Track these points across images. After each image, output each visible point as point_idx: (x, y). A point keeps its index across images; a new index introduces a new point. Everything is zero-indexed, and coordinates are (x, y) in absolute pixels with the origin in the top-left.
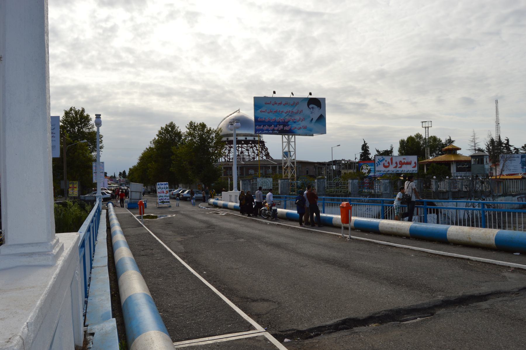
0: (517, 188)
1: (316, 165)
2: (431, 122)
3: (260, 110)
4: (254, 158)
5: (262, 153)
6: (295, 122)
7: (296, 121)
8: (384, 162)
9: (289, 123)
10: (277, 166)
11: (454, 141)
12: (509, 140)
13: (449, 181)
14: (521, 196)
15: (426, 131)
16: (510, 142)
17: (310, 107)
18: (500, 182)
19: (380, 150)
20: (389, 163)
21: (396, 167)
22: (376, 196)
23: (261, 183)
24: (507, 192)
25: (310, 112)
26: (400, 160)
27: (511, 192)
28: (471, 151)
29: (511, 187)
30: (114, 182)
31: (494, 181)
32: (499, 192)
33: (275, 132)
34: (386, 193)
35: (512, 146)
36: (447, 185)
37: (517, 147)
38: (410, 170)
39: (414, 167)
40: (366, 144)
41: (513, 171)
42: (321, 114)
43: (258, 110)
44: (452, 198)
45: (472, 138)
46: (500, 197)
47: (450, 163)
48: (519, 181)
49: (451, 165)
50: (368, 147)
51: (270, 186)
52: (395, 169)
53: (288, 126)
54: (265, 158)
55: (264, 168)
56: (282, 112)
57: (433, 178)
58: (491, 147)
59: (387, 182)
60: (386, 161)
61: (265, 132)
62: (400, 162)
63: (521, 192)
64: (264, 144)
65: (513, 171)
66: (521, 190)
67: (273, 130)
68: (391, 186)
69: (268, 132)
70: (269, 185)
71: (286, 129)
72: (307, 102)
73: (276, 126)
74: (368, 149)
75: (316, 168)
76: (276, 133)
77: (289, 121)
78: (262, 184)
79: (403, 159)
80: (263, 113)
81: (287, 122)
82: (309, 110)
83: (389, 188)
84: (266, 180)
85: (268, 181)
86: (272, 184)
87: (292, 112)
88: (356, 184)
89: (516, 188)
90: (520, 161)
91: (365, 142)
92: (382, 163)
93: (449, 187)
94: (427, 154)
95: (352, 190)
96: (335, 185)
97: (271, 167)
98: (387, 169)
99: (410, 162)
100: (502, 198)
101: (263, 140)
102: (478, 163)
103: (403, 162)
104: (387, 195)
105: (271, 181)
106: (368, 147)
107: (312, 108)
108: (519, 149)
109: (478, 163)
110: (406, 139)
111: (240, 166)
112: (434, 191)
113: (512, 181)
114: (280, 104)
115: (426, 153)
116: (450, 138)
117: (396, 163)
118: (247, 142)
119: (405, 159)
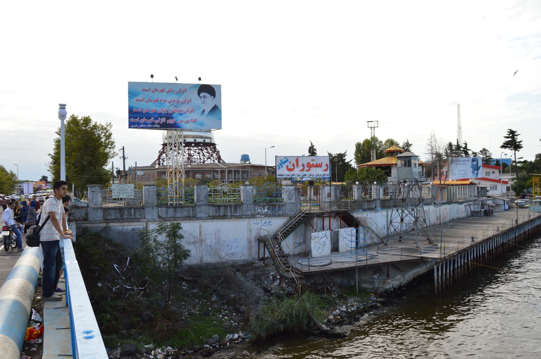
0: (464, 194)
1: (270, 169)
2: (377, 121)
3: (136, 98)
4: (204, 162)
5: (213, 156)
6: (181, 114)
7: (183, 112)
8: (288, 163)
9: (174, 115)
10: (225, 170)
11: (412, 144)
12: (467, 144)
13: (377, 187)
14: (469, 203)
15: (372, 132)
16: (468, 146)
17: (200, 96)
18: (444, 188)
19: (332, 153)
20: (293, 165)
21: (303, 170)
22: (277, 206)
23: (118, 191)
24: (452, 199)
25: (201, 101)
26: (308, 162)
27: (458, 199)
28: (428, 155)
29: (463, 194)
30: (49, 186)
31: (436, 187)
32: (442, 199)
33: (156, 126)
34: (290, 203)
35: (470, 150)
36: (374, 192)
37: (475, 152)
38: (320, 174)
39: (326, 170)
40: (313, 146)
41: (463, 175)
42: (216, 105)
43: (133, 98)
44: (381, 208)
45: (430, 141)
46: (444, 205)
47: (391, 166)
48: (467, 187)
49: (392, 168)
50: (316, 149)
51: (130, 194)
52: (301, 173)
53: (172, 118)
54: (216, 161)
55: (212, 173)
56: (165, 101)
57: (355, 184)
58: (449, 151)
59: (292, 188)
60: (290, 163)
61: (142, 126)
62: (307, 165)
63: (469, 199)
64: (216, 147)
65: (463, 175)
66: (469, 196)
67: (153, 123)
68: (297, 194)
69: (146, 125)
70: (128, 193)
71: (170, 122)
72: (198, 89)
73: (157, 119)
74: (316, 152)
75: (270, 173)
76: (157, 127)
77: (174, 113)
78: (119, 191)
79: (312, 160)
80: (139, 102)
81: (171, 114)
82: (200, 99)
83: (294, 195)
84: (124, 186)
85: (127, 187)
86: (133, 192)
87: (177, 101)
88: (250, 191)
89: (463, 195)
90: (471, 165)
91: (312, 144)
92: (285, 166)
93: (377, 194)
94: (373, 157)
95: (245, 199)
96: (222, 193)
97: (219, 171)
98: (291, 173)
99: (320, 164)
100: (447, 206)
101: (215, 143)
102: (405, 166)
103: (311, 164)
104: (292, 204)
105: (132, 188)
106: (316, 149)
107: (203, 96)
108: (477, 153)
109: (405, 166)
110: (362, 142)
111: (220, 169)
112: (356, 199)
113: (459, 188)
114: (162, 91)
115: (372, 156)
116: (408, 141)
117: (303, 165)
118: (197, 144)
119: (314, 160)
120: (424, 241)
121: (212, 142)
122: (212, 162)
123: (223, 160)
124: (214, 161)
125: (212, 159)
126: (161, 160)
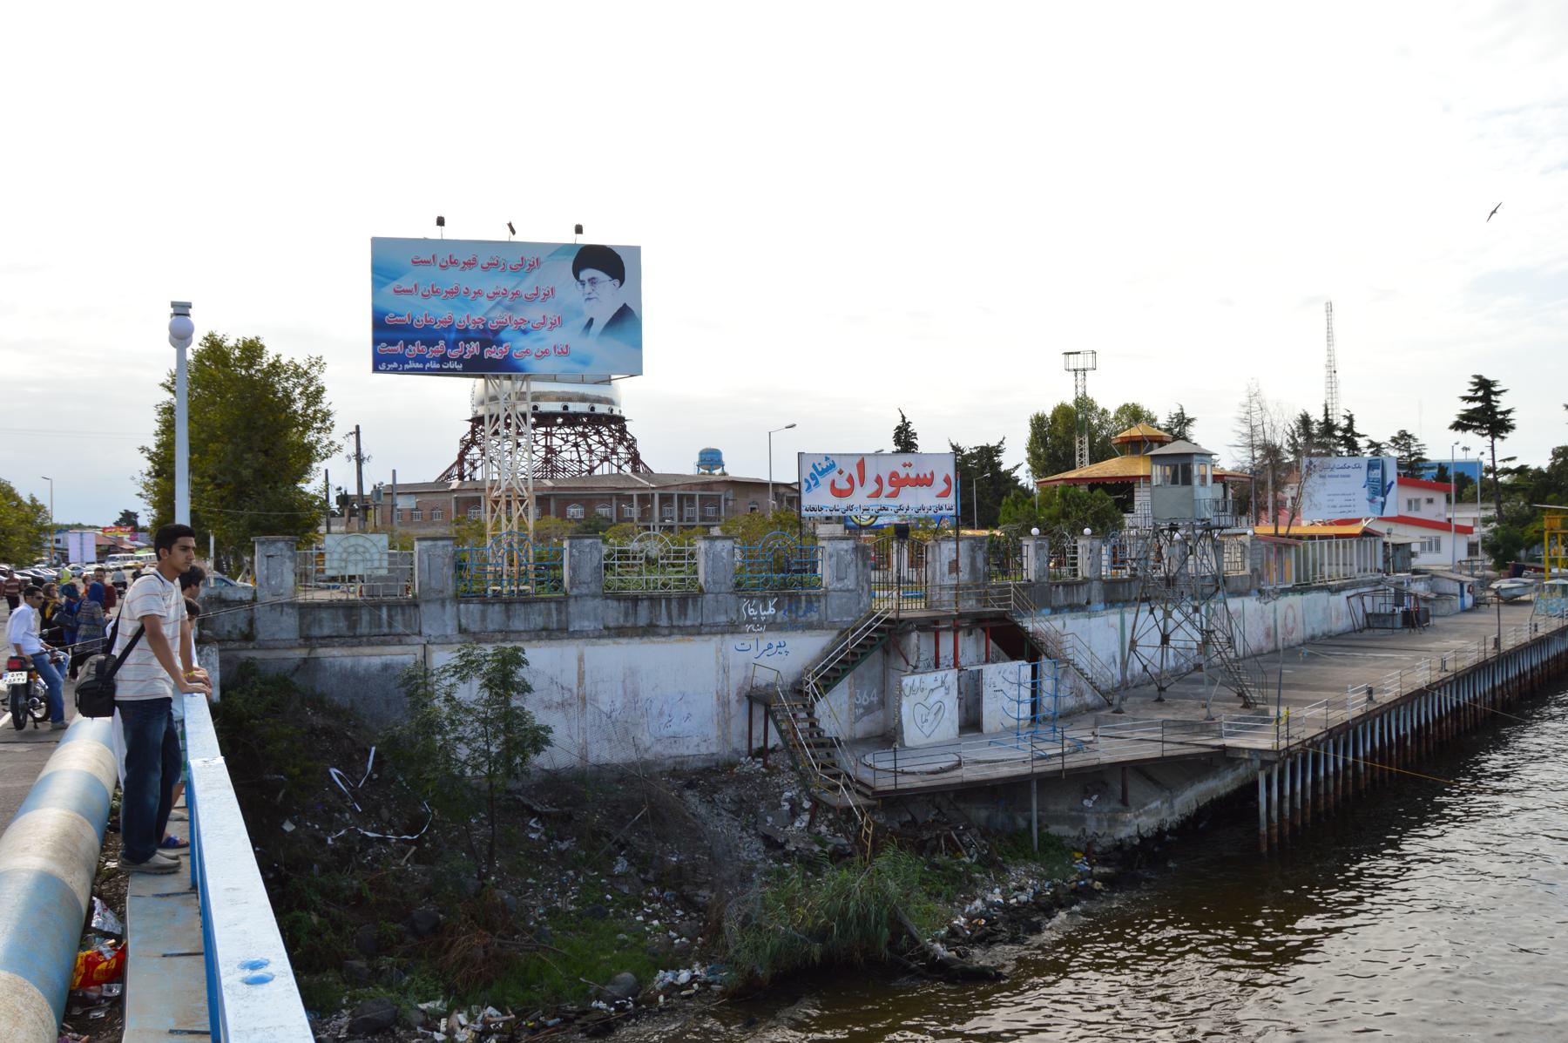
0: (1345, 564)
1: (782, 490)
2: (1094, 352)
3: (394, 284)
4: (592, 470)
5: (617, 454)
6: (525, 332)
7: (529, 326)
8: (834, 474)
9: (503, 335)
10: (653, 495)
11: (1193, 419)
12: (1355, 418)
13: (1091, 544)
14: (1360, 590)
15: (1080, 383)
16: (1355, 424)
17: (581, 278)
18: (1288, 546)
19: (962, 445)
20: (850, 479)
21: (877, 494)
22: (803, 598)
23: (341, 554)
24: (1311, 578)
25: (584, 295)
26: (894, 469)
27: (1327, 578)
28: (1240, 449)
29: (1341, 563)
30: (142, 541)
31: (1263, 543)
32: (1282, 579)
33: (451, 365)
34: (841, 590)
35: (1364, 436)
36: (1085, 558)
37: (1376, 440)
38: (927, 505)
39: (944, 494)
40: (908, 424)
41: (1343, 509)
42: (625, 305)
43: (386, 284)
44: (1105, 604)
45: (1246, 409)
46: (1286, 595)
47: (1133, 484)
48: (1355, 542)
49: (1136, 490)
50: (915, 434)
51: (377, 564)
52: (873, 501)
53: (499, 343)
54: (627, 469)
55: (614, 501)
56: (478, 293)
57: (1030, 533)
58: (1300, 440)
59: (845, 547)
60: (841, 472)
61: (412, 365)
62: (891, 478)
63: (1358, 579)
64: (625, 426)
65: (1343, 509)
66: (1359, 571)
67: (444, 359)
68: (860, 563)
69: (424, 364)
70: (372, 561)
71: (494, 356)
72: (573, 258)
73: (455, 345)
74: (914, 440)
75: (782, 501)
76: (455, 370)
77: (503, 328)
78: (344, 556)
79: (905, 465)
80: (403, 297)
81: (497, 332)
82: (580, 287)
83: (853, 566)
84: (360, 541)
85: (368, 544)
86: (386, 557)
87: (514, 294)
88: (724, 554)
89: (1341, 566)
90: (1365, 478)
91: (903, 417)
92: (825, 481)
93: (1092, 565)
94: (1081, 456)
95: (709, 579)
96: (643, 561)
97: (635, 498)
98: (843, 503)
99: (929, 476)
100: (1295, 600)
101: (622, 414)
102: (1174, 482)
103: (902, 475)
104: (847, 594)
105: (384, 547)
106: (915, 434)
107: (589, 280)
108: (1383, 446)
109: (1174, 482)
110: (1049, 414)
111: (639, 492)
112: (1033, 580)
113: (1329, 546)
114: (470, 264)
115: (1077, 454)
116: (1182, 409)
117: (879, 480)
118: (571, 420)
119: (910, 465)
120: (1228, 700)
121: (614, 413)
122: (615, 470)
123: (645, 466)
124: (619, 467)
125: (615, 462)
126: (466, 465)
